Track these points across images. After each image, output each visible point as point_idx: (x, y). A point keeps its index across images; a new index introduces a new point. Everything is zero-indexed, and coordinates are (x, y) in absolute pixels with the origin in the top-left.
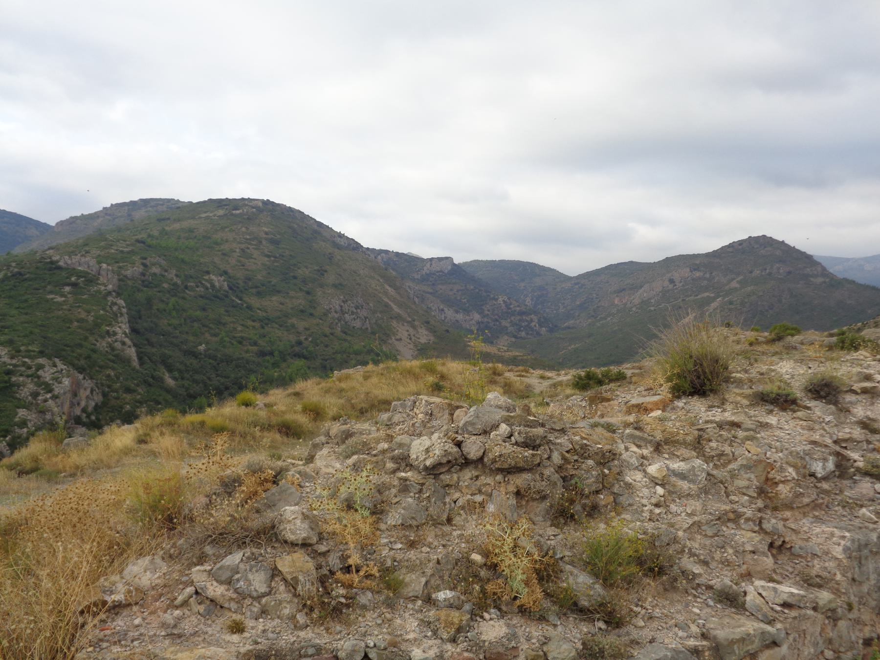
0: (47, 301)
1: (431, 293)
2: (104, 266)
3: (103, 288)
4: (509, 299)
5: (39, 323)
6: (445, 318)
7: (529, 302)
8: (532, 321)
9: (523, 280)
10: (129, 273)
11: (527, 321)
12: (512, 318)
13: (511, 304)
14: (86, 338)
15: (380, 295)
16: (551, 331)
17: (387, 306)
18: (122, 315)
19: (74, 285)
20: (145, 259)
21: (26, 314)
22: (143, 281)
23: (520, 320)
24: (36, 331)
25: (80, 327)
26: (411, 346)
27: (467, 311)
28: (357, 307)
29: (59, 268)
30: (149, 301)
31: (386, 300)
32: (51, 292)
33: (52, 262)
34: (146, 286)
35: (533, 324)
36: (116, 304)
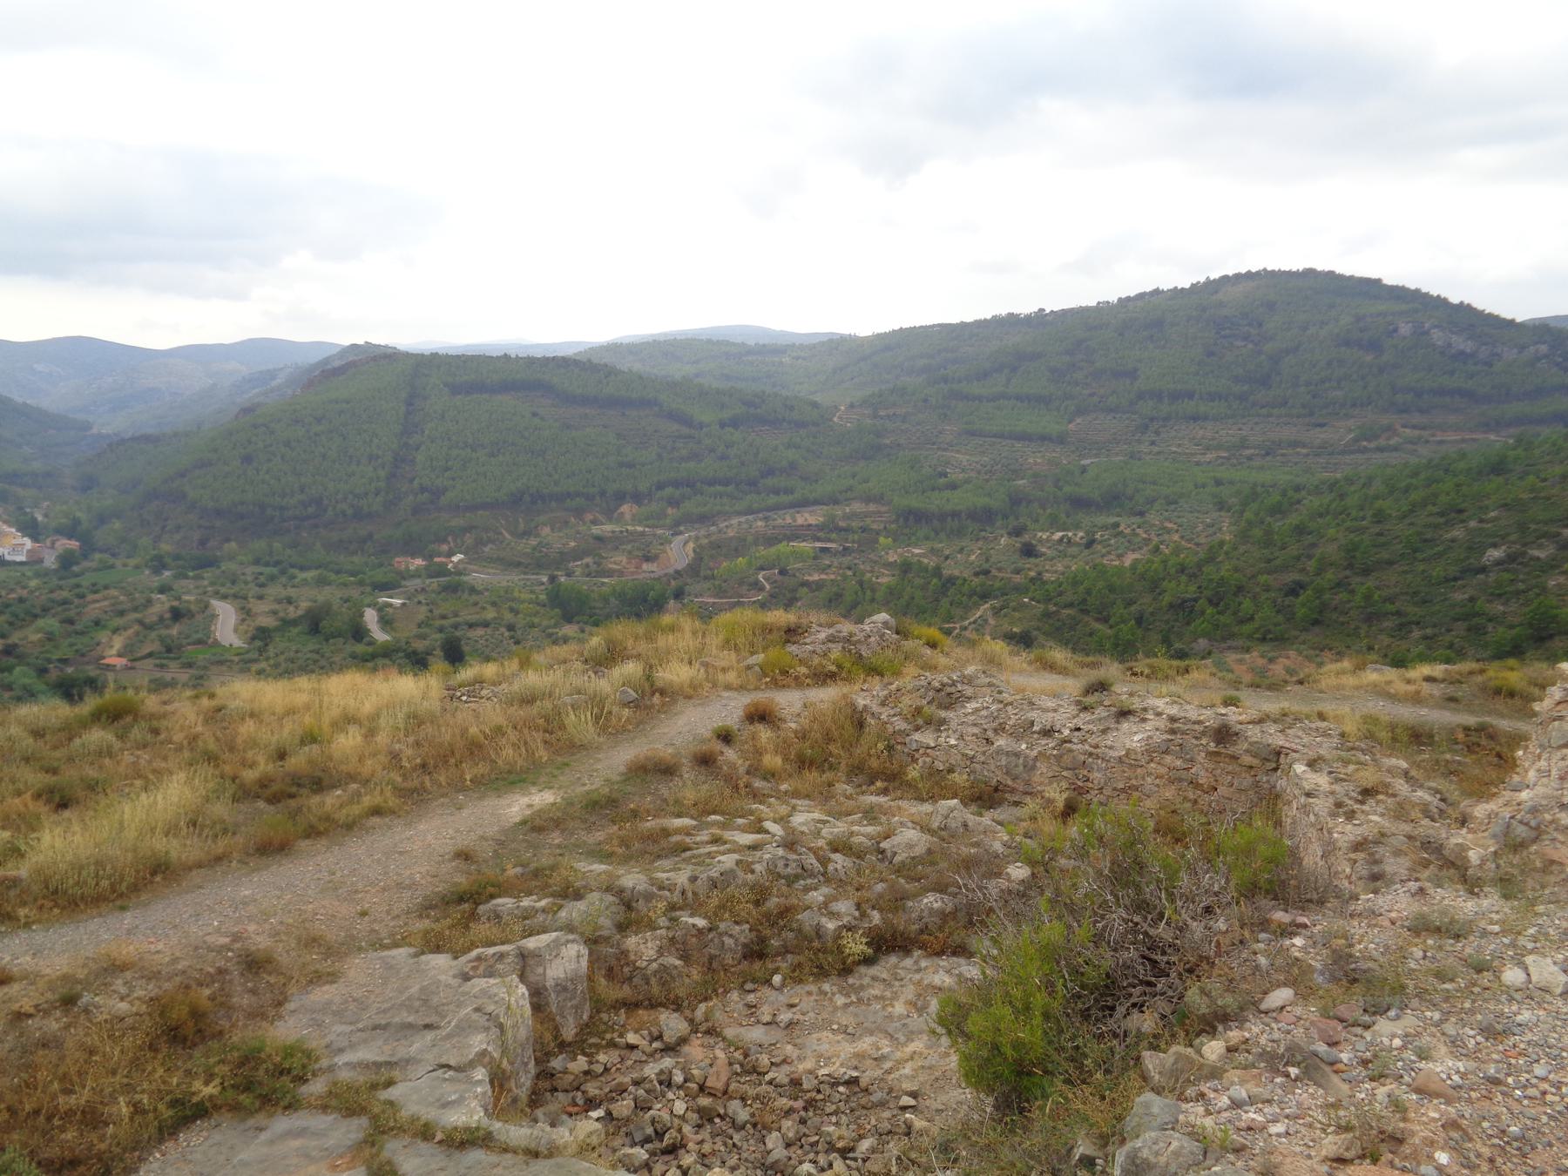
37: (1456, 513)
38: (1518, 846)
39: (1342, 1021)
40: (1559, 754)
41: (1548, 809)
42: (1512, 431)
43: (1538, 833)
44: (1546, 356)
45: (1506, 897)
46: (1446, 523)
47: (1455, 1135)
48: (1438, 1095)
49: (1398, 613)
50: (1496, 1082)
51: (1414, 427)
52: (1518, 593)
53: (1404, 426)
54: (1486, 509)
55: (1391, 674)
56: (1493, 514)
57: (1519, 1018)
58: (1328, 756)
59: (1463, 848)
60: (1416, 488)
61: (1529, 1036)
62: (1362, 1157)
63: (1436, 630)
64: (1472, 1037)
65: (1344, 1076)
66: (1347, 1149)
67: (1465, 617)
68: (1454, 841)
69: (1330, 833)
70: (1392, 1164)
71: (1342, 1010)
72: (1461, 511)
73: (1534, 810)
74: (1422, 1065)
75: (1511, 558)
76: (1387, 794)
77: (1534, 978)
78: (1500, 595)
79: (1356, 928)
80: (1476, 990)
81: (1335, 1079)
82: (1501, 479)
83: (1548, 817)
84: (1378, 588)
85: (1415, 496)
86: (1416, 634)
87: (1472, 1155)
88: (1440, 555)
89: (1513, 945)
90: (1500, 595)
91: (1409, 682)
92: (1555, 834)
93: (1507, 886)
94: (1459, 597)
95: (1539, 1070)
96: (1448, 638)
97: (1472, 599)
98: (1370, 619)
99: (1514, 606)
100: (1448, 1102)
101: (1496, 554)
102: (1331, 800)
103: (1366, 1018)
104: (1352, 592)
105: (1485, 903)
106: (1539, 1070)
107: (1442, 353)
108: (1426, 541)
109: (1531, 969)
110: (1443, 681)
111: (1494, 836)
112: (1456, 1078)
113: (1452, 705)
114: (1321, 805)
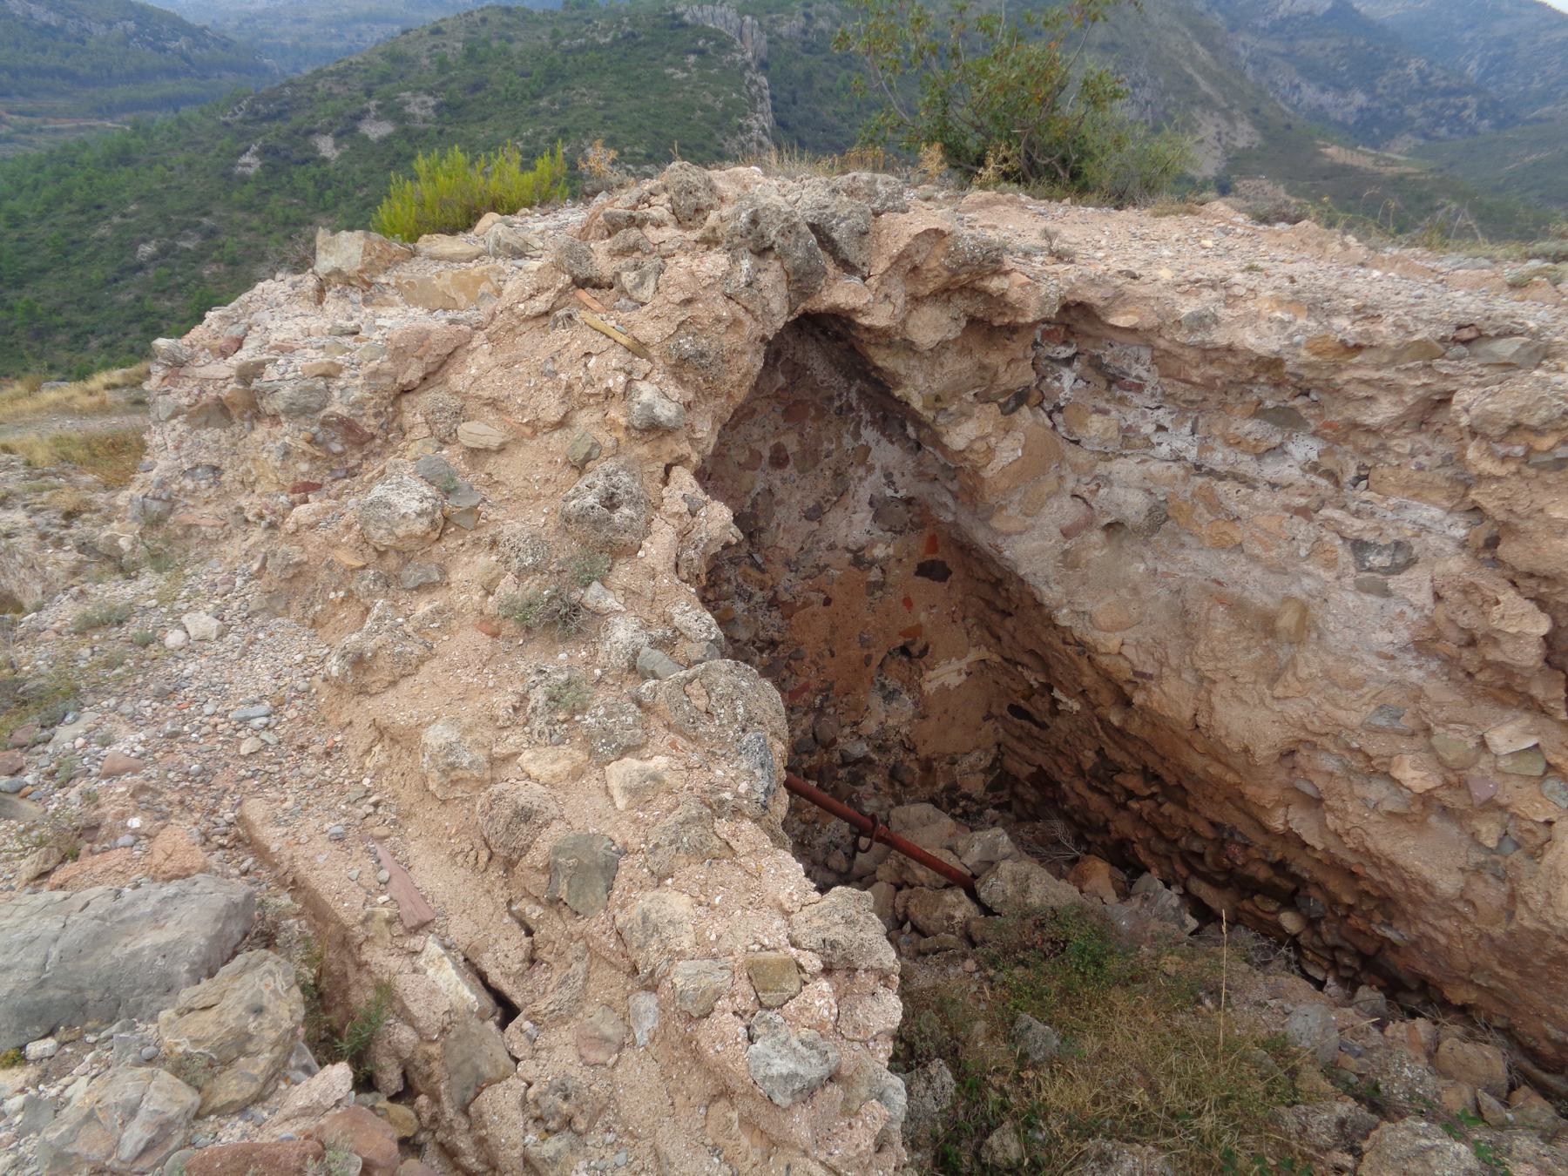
0: (665, 78)
1: (1282, 56)
2: (748, 19)
3: (739, 57)
4: (1430, 64)
5: (652, 111)
6: (1300, 100)
7: (1473, 70)
8: (1465, 106)
9: (1471, 27)
10: (784, 30)
11: (1456, 107)
12: (1429, 101)
13: (1431, 74)
14: (712, 135)
15: (1181, 61)
16: (1500, 125)
17: (1189, 81)
18: (762, 98)
19: (701, 52)
20: (810, 6)
21: (637, 97)
22: (804, 43)
23: (1442, 106)
24: (647, 123)
25: (703, 119)
26: (1218, 153)
27: (1342, 89)
28: (1134, 85)
29: (684, 25)
30: (809, 78)
31: (1189, 70)
32: (670, 64)
33: (675, 17)
34: (809, 52)
35: (1467, 112)
36: (755, 82)
37: (94, 209)
38: (156, 522)
39: (21, 747)
40: (169, 427)
41: (173, 479)
42: (127, 117)
43: (171, 503)
44: (136, 35)
45: (159, 571)
46: (89, 221)
47: (146, 797)
48: (124, 771)
49: (69, 324)
50: (174, 735)
51: (21, 113)
52: (179, 286)
53: (10, 112)
54: (124, 203)
55: (71, 389)
56: (133, 207)
57: (186, 673)
58: (19, 490)
59: (113, 539)
60: (45, 184)
61: (196, 684)
62: (63, 861)
63: (113, 337)
64: (147, 706)
65: (32, 797)
66: (46, 862)
67: (139, 318)
68: (104, 535)
69: (43, 568)
70: (92, 852)
71: (21, 736)
72: (99, 207)
73: (162, 484)
74: (107, 751)
75: (164, 252)
76: (90, 511)
77: (192, 633)
78: (163, 291)
79: (21, 653)
80: (144, 664)
81: (25, 804)
82: (130, 170)
83: (175, 487)
84: (38, 300)
85: (48, 192)
86: (94, 343)
87: (163, 807)
88: (93, 256)
89: (171, 611)
90: (163, 291)
91: (91, 394)
92: (186, 501)
93: (158, 560)
94: (125, 298)
95: (208, 709)
96: (126, 342)
97: (138, 299)
98: (39, 335)
99: (179, 301)
100: (136, 772)
101: (147, 249)
102: (34, 534)
103: (46, 733)
104: (11, 308)
105: (143, 583)
106: (208, 709)
107: (25, 25)
108: (74, 242)
109: (189, 626)
110: (125, 385)
111: (135, 519)
112: (139, 748)
113: (140, 408)
114: (26, 542)
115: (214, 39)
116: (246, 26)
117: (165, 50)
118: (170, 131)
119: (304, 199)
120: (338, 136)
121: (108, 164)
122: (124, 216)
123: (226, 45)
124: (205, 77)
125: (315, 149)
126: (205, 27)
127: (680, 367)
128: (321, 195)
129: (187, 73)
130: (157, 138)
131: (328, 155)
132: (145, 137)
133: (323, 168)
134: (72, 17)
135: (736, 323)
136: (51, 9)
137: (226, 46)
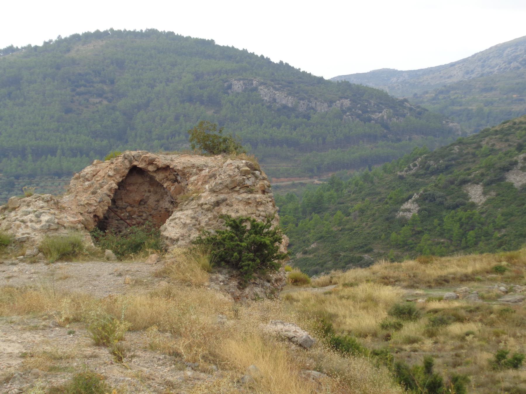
44: (349, 109)
54: (307, 242)
56: (313, 246)
107: (269, 107)
115: (411, 109)
116: (441, 97)
117: (369, 120)
118: (356, 185)
119: (450, 239)
120: (487, 184)
121: (304, 212)
122: (305, 253)
123: (420, 113)
124: (399, 140)
125: (466, 196)
126: (406, 100)
127: (115, 170)
128: (464, 235)
129: (385, 136)
130: (345, 191)
131: (476, 201)
132: (337, 190)
133: (469, 212)
134: (303, 99)
135: (121, 166)
136: (289, 94)
137: (420, 113)
